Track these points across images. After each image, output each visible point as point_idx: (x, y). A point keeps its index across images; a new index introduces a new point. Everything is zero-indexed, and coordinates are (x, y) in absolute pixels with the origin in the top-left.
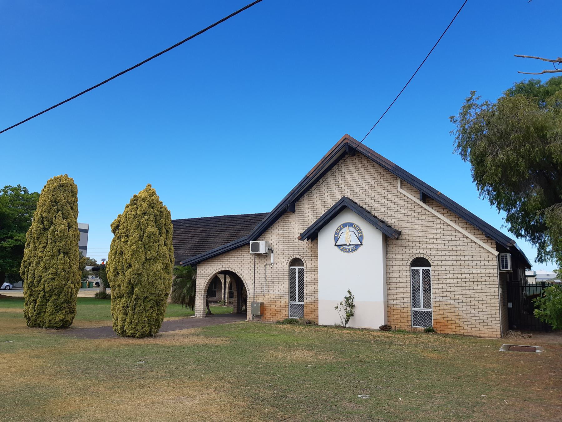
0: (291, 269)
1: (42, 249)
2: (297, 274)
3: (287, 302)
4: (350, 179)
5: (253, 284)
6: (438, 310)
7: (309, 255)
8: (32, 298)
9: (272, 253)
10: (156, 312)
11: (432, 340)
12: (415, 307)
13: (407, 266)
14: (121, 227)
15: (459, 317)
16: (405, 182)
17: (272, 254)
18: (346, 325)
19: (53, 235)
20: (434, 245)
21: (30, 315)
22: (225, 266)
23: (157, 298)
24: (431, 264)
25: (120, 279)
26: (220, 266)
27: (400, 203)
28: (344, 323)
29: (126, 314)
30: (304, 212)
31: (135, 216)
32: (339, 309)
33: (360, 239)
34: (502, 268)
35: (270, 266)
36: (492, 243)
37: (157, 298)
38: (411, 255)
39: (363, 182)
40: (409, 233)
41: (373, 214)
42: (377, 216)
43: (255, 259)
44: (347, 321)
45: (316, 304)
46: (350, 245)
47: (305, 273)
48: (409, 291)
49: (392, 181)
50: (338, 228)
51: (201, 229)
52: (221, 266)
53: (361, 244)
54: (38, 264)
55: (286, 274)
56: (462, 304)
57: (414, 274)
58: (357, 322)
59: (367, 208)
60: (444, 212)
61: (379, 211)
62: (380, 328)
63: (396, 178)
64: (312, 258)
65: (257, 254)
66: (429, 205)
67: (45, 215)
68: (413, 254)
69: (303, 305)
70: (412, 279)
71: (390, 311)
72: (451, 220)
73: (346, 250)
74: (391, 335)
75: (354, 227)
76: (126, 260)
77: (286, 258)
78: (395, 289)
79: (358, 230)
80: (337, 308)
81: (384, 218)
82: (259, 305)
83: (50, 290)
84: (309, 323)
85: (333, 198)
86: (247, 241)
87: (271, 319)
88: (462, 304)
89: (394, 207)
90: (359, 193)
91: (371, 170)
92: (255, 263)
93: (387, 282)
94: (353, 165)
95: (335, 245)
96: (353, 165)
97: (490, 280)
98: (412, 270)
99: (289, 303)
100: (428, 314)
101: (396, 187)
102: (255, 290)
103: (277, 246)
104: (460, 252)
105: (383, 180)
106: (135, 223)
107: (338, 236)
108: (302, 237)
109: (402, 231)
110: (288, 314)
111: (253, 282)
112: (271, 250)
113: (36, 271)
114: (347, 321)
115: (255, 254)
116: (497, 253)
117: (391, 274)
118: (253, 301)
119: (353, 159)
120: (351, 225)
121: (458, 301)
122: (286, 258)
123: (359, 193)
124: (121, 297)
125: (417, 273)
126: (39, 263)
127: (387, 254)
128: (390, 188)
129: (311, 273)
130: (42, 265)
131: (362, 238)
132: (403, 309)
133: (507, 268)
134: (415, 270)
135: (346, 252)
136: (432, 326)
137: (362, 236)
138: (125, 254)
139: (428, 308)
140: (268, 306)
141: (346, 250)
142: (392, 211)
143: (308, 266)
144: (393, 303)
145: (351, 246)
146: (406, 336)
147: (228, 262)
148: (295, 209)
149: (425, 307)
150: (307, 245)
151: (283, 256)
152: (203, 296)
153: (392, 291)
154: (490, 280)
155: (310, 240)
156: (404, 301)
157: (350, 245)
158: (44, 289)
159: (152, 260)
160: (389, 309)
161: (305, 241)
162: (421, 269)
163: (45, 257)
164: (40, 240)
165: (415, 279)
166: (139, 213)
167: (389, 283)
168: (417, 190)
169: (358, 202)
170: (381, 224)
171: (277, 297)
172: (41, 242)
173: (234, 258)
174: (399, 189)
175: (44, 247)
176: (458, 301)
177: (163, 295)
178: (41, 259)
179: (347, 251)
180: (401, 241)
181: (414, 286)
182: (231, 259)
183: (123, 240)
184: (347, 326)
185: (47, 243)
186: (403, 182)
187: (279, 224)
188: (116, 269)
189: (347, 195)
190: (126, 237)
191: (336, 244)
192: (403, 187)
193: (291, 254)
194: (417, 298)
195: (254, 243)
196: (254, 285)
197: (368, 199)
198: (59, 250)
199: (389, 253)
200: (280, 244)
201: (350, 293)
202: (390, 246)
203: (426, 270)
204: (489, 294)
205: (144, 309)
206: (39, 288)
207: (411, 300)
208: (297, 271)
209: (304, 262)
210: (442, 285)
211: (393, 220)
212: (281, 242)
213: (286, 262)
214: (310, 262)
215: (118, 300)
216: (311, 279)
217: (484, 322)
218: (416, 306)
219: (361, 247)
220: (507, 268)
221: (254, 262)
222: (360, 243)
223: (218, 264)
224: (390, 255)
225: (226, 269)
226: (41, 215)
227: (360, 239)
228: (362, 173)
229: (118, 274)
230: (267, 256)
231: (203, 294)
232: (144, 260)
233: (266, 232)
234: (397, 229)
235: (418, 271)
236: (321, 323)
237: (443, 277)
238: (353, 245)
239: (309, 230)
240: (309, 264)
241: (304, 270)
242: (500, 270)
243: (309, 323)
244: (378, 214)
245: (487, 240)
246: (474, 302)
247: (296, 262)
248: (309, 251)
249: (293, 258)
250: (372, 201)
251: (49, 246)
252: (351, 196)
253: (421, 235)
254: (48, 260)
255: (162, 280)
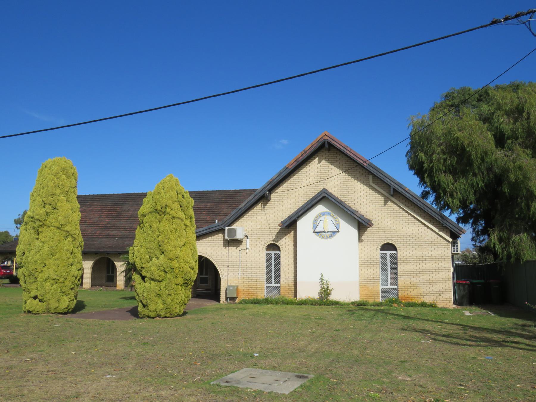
2: (273, 258)
4: (326, 171)
5: (227, 268)
34: (454, 252)
51: (108, 208)
60: (409, 205)
61: (353, 202)
66: (396, 199)
68: (382, 240)
77: (262, 243)
81: (357, 208)
86: (222, 226)
88: (423, 281)
90: (335, 185)
94: (328, 159)
95: (314, 232)
96: (328, 159)
97: (445, 262)
104: (422, 238)
119: (328, 154)
121: (420, 279)
122: (262, 243)
123: (335, 185)
131: (339, 226)
133: (457, 252)
137: (339, 224)
141: (324, 236)
142: (364, 202)
151: (259, 241)
154: (445, 262)
176: (420, 279)
193: (267, 239)
195: (229, 228)
197: (343, 191)
208: (273, 256)
210: (407, 266)
213: (262, 247)
220: (457, 252)
222: (337, 231)
225: (394, 244)
237: (407, 259)
238: (330, 232)
240: (286, 249)
244: (352, 204)
246: (432, 279)
253: (389, 224)
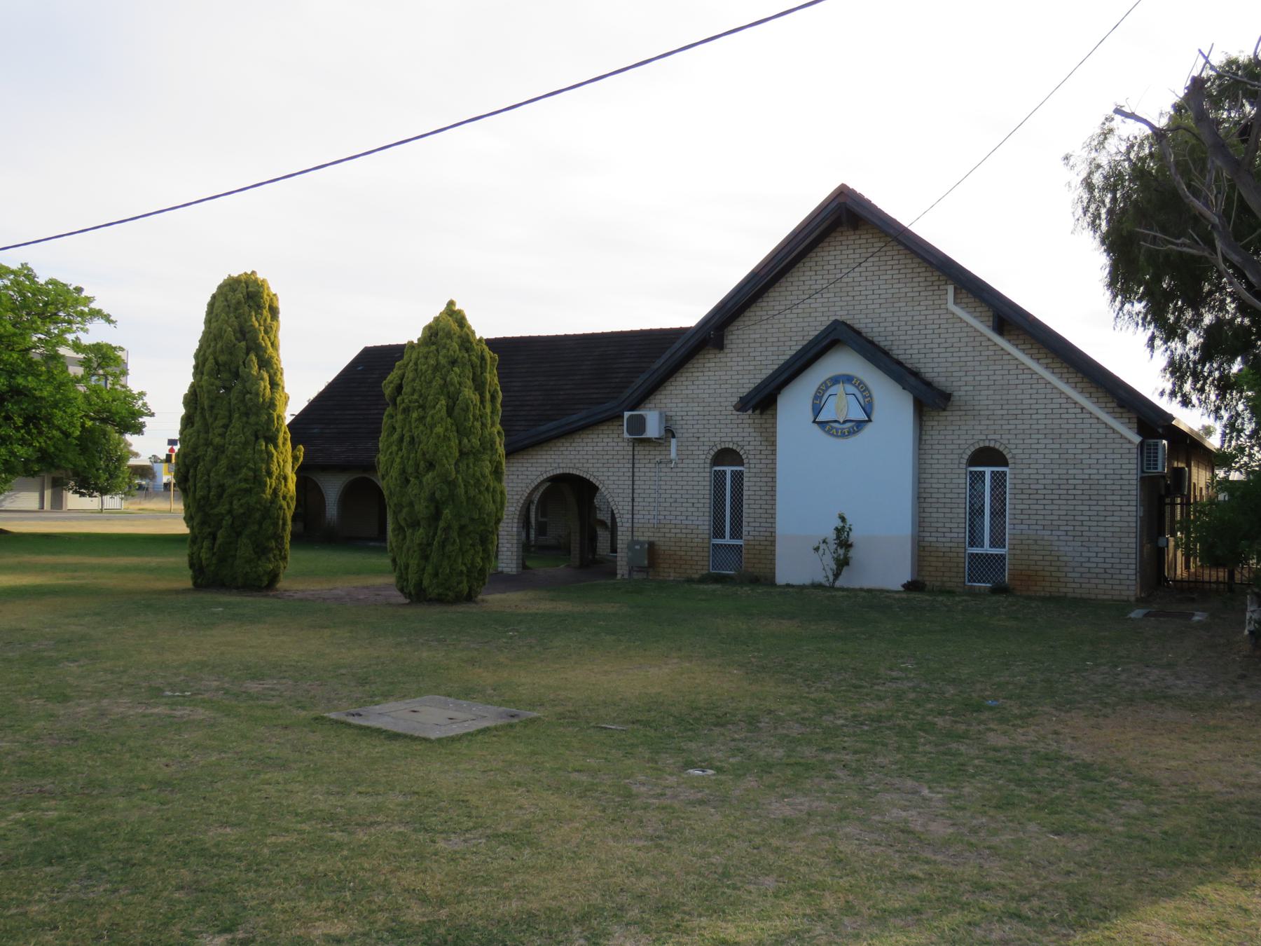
0: (715, 471)
1: (220, 431)
3: (706, 541)
5: (631, 504)
6: (1018, 552)
7: (756, 443)
8: (207, 530)
9: (674, 436)
10: (481, 554)
11: (1006, 604)
12: (972, 546)
13: (961, 466)
14: (406, 389)
15: (1058, 564)
16: (964, 291)
17: (673, 441)
18: (834, 583)
19: (243, 401)
20: (1017, 422)
21: (204, 563)
22: (564, 465)
23: (482, 528)
24: (1010, 461)
25: (412, 490)
26: (553, 465)
27: (951, 335)
28: (831, 578)
29: (426, 558)
30: (746, 350)
31: (436, 368)
32: (821, 551)
33: (868, 409)
34: (1148, 468)
35: (668, 465)
36: (1129, 418)
37: (482, 528)
38: (970, 442)
39: (874, 287)
40: (967, 398)
41: (896, 357)
42: (904, 361)
43: (633, 450)
44: (837, 575)
45: (769, 543)
46: (845, 422)
47: (745, 479)
48: (963, 516)
49: (937, 288)
50: (822, 385)
52: (556, 465)
53: (870, 420)
54: (216, 460)
55: (705, 483)
56: (1066, 538)
57: (973, 482)
58: (859, 578)
59: (882, 344)
60: (1039, 356)
62: (904, 586)
63: (943, 283)
64: (760, 448)
65: (640, 439)
66: (1009, 341)
67: (222, 358)
69: (741, 546)
70: (970, 490)
71: (922, 554)
72: (1053, 373)
73: (837, 432)
74: (927, 597)
75: (854, 385)
76: (424, 454)
78: (935, 510)
79: (864, 391)
80: (817, 549)
82: (646, 546)
83: (244, 514)
84: (755, 580)
85: (810, 319)
87: (672, 574)
88: (1066, 538)
89: (939, 344)
91: (892, 263)
92: (633, 459)
93: (919, 498)
94: (854, 250)
95: (814, 422)
98: (971, 472)
99: (709, 543)
100: (989, 558)
101: (944, 302)
102: (635, 516)
103: (685, 422)
105: (917, 284)
106: (438, 382)
107: (820, 402)
108: (744, 405)
109: (955, 394)
110: (709, 565)
111: (630, 499)
112: (670, 432)
113: (212, 475)
114: (837, 575)
115: (634, 439)
116: (1137, 439)
117: (927, 481)
118: (630, 538)
119: (853, 237)
120: (848, 379)
121: (1059, 533)
124: (415, 524)
125: (980, 479)
126: (217, 458)
127: (920, 439)
128: (931, 303)
129: (759, 479)
130: (223, 462)
132: (949, 550)
133: (1156, 468)
134: (976, 472)
135: (837, 436)
136: (1004, 581)
137: (871, 404)
138: (420, 443)
139: (999, 547)
140: (663, 548)
141: (837, 432)
143: (752, 466)
144: (930, 539)
145: (848, 425)
146: (957, 599)
147: (572, 457)
148: (725, 342)
149: (992, 545)
150: (752, 421)
151: (698, 443)
152: (515, 529)
153: (928, 515)
155: (758, 412)
156: (952, 535)
157: (845, 422)
158: (230, 512)
159: (471, 456)
160: (921, 550)
161: (750, 412)
162: (988, 470)
163: (231, 447)
164: (215, 411)
165: (975, 490)
166: (442, 362)
167: (922, 500)
168: (987, 309)
169: (863, 331)
170: (912, 380)
171: (684, 531)
172: (217, 414)
173: (585, 449)
174: (952, 307)
175: (226, 426)
177: (492, 524)
178: (220, 449)
179: (839, 434)
180: (950, 413)
181: (973, 505)
182: (578, 449)
183: (415, 415)
184: (838, 584)
185: (230, 418)
186: (959, 291)
187: (687, 374)
188: (403, 471)
189: (842, 315)
190: (420, 410)
191: (815, 419)
192: (959, 301)
194: (977, 529)
196: (633, 506)
198: (256, 432)
199: (924, 437)
200: (691, 418)
201: (843, 519)
202: (927, 423)
203: (998, 472)
204: (1118, 519)
205: (461, 549)
206: (222, 509)
207: (965, 533)
209: (744, 457)
211: (934, 369)
212: (692, 413)
213: (704, 457)
214: (758, 457)
215: (409, 532)
216: (760, 493)
217: (1106, 572)
218: (974, 543)
219: (870, 424)
220: (1156, 468)
221: (631, 457)
222: (867, 419)
223: (549, 461)
224: (927, 442)
225: (567, 471)
226: (215, 358)
227: (867, 409)
228: (873, 269)
229: (408, 481)
230: (660, 444)
231: (515, 525)
232: (457, 454)
233: (658, 392)
234: (944, 388)
235: (983, 474)
236: (781, 579)
239: (758, 389)
241: (743, 474)
242: (1143, 471)
243: (755, 580)
245: (1121, 413)
247: (726, 456)
248: (755, 434)
249: (719, 448)
250: (893, 329)
251: (236, 424)
252: (849, 317)
254: (236, 453)
255: (490, 495)
